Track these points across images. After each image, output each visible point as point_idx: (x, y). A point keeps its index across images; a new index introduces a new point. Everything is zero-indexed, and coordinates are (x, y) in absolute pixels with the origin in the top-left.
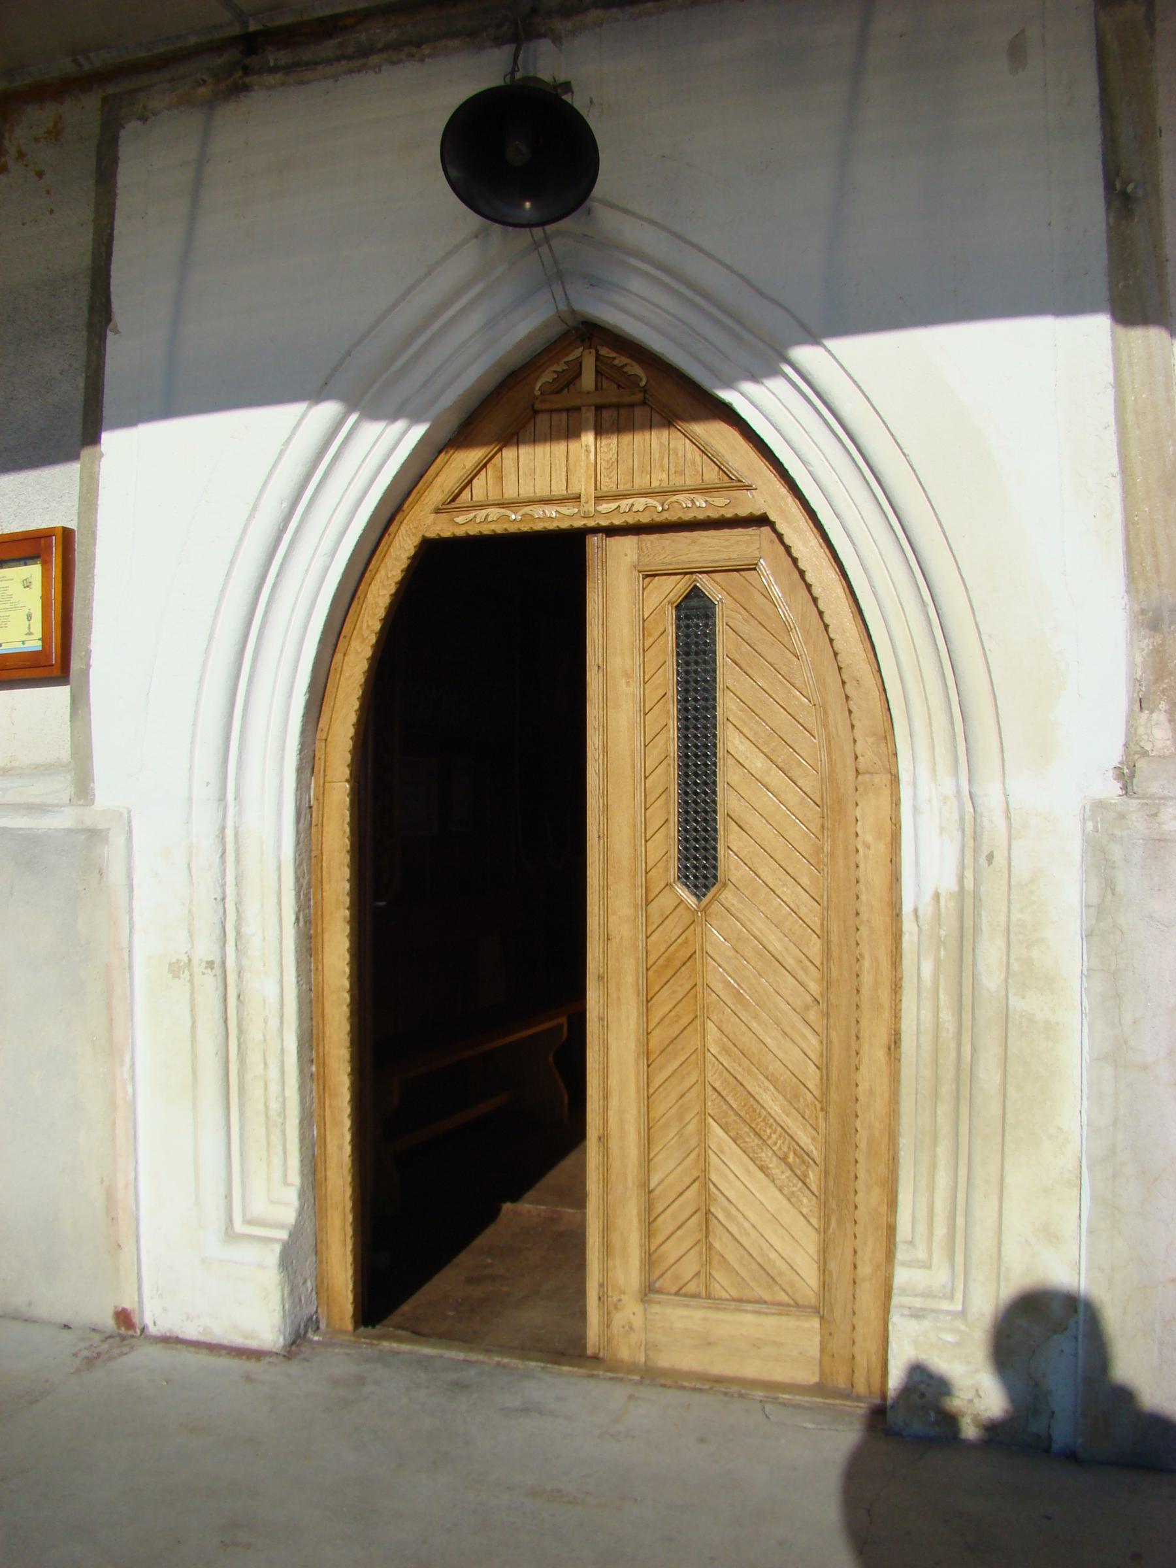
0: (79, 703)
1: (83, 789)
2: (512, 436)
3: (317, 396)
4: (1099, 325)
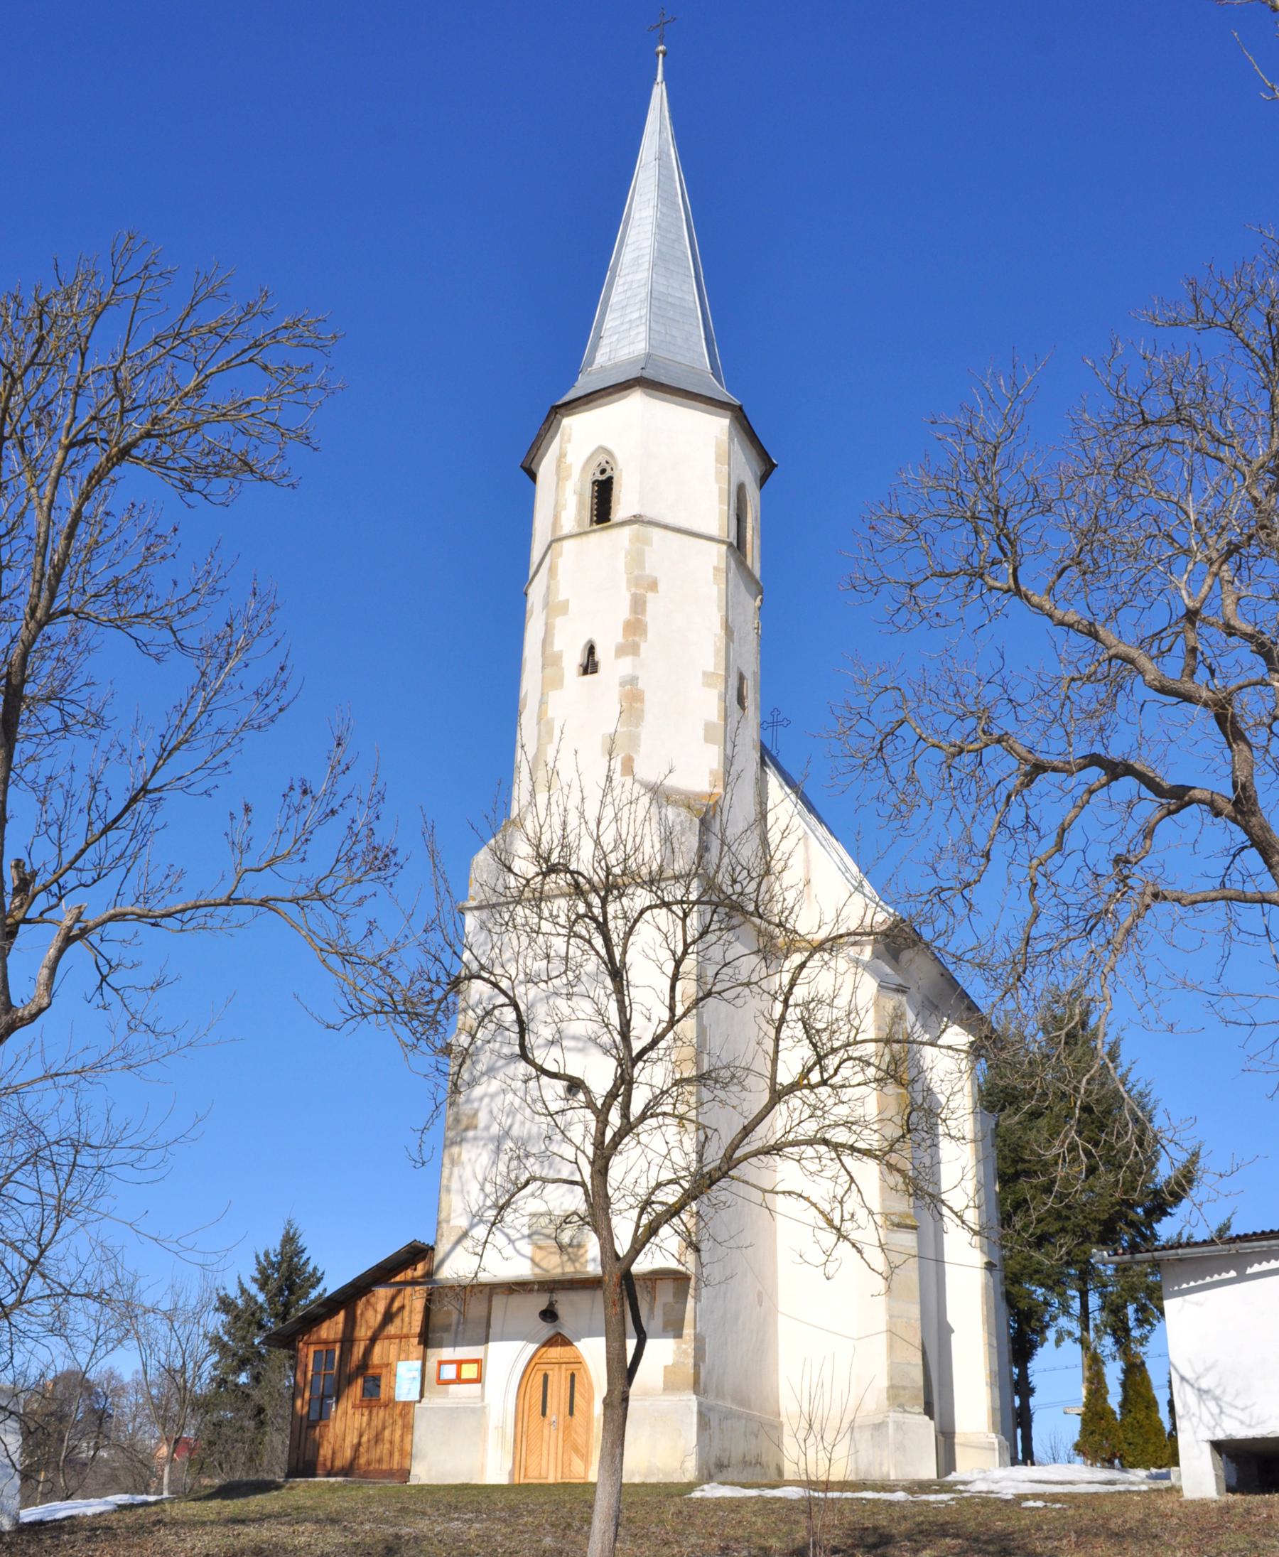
0: (483, 1387)
2: (551, 1346)
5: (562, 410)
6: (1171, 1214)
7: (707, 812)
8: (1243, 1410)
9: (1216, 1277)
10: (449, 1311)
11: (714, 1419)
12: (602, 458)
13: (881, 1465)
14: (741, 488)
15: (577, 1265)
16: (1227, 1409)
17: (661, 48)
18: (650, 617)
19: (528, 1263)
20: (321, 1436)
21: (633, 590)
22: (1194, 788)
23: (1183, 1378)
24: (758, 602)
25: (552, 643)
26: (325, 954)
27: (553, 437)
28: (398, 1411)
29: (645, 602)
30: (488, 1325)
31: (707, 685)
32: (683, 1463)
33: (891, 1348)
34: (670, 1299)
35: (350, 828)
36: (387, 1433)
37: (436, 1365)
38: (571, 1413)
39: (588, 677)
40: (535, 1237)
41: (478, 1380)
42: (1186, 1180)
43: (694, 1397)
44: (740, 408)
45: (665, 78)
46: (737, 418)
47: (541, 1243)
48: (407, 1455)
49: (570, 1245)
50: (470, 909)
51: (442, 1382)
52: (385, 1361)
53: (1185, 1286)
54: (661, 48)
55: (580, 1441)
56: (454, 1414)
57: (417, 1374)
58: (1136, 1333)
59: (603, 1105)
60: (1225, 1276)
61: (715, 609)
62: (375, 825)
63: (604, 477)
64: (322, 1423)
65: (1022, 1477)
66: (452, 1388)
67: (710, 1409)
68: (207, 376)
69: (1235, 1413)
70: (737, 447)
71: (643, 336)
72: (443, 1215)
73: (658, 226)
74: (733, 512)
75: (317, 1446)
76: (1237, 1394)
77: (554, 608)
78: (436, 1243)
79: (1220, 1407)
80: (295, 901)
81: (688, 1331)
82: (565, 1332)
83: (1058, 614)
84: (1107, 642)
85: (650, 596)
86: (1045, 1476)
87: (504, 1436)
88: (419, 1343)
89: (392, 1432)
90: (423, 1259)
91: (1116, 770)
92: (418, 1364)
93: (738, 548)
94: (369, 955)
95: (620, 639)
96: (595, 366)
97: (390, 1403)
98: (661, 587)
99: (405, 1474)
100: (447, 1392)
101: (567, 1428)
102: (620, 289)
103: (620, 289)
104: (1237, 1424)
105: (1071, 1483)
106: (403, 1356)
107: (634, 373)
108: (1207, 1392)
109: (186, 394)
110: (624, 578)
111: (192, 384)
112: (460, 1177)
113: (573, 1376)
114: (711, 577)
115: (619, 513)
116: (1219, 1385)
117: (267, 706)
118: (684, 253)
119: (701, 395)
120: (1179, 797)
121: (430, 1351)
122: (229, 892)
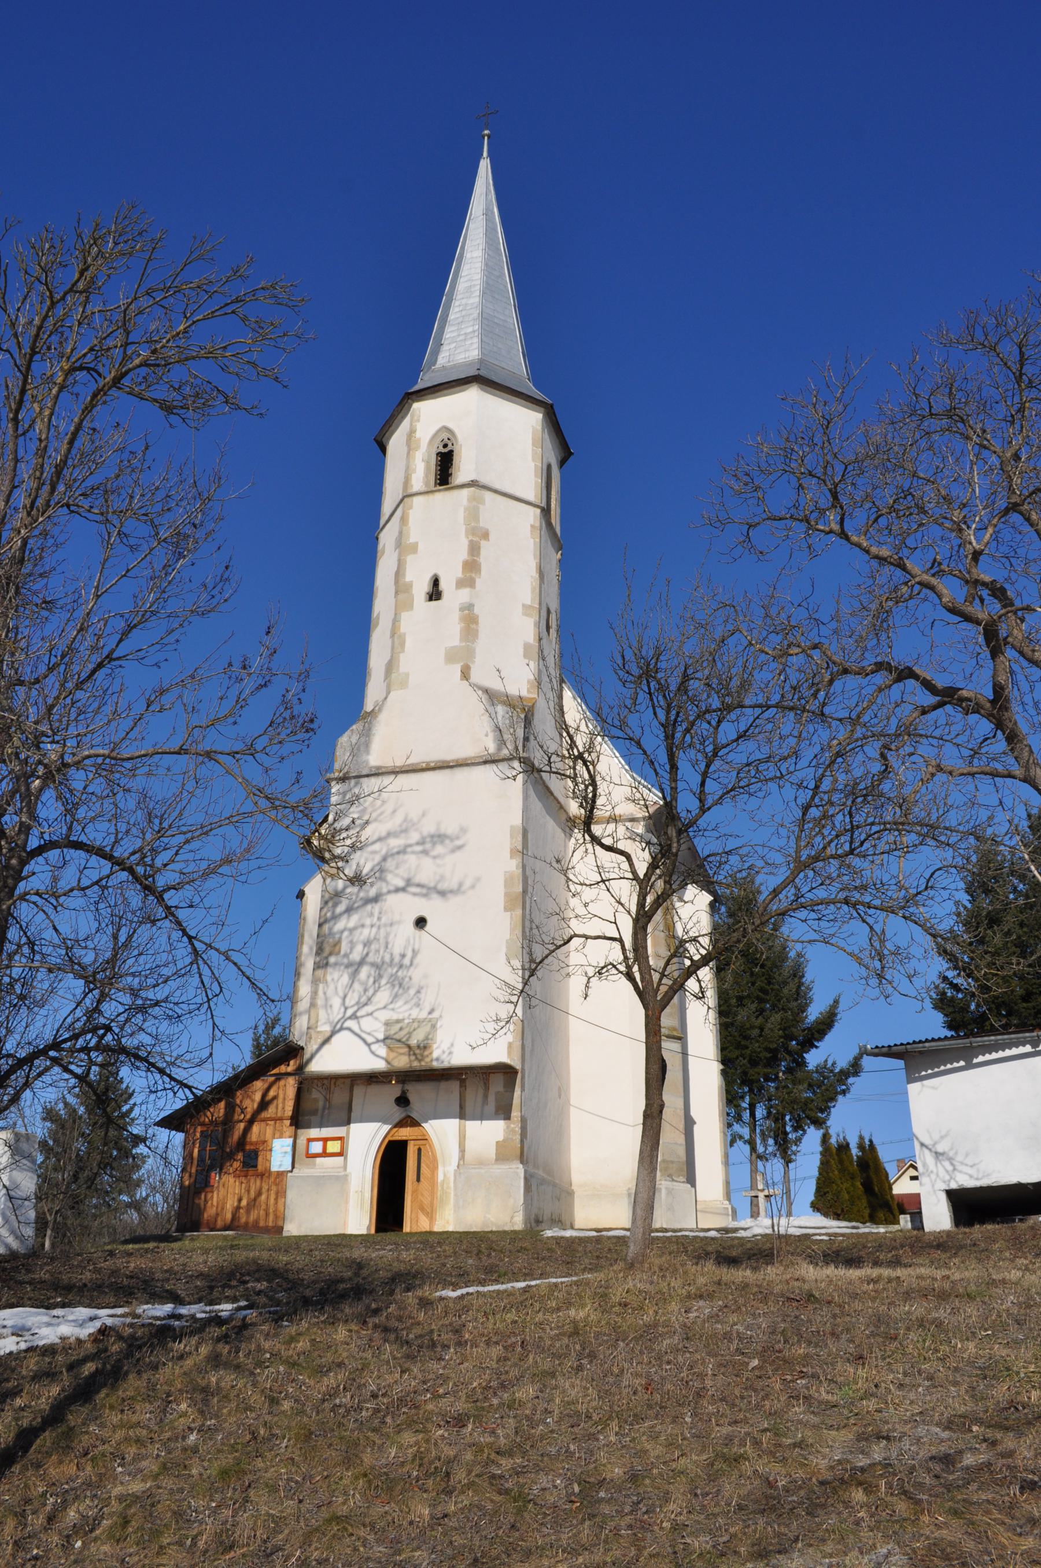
0: (346, 1159)
4: (457, 1120)
5: (414, 397)
6: (817, 1047)
9: (949, 1066)
11: (534, 1182)
12: (445, 435)
14: (549, 467)
16: (959, 1167)
17: (486, 132)
20: (206, 1201)
21: (471, 537)
23: (922, 1145)
24: (559, 556)
25: (404, 575)
26: (257, 798)
27: (403, 418)
28: (272, 1179)
29: (479, 548)
31: (525, 614)
32: (512, 1218)
34: (501, 1089)
35: (284, 696)
36: (263, 1197)
37: (305, 1142)
38: (418, 1180)
39: (433, 603)
40: (388, 1041)
42: (826, 1023)
43: (521, 1166)
44: (552, 406)
45: (489, 155)
48: (280, 1217)
49: (419, 1047)
52: (262, 1138)
53: (923, 1073)
55: (426, 1201)
56: (321, 1181)
57: (289, 1149)
58: (792, 1136)
59: (645, 875)
60: (956, 1065)
61: (532, 557)
62: (301, 696)
63: (446, 450)
66: (318, 1160)
67: (532, 1176)
68: (194, 322)
70: (546, 436)
71: (476, 345)
73: (486, 265)
74: (544, 485)
77: (404, 548)
80: (233, 754)
81: (515, 1114)
82: (414, 1115)
83: (874, 550)
84: (913, 572)
85: (483, 543)
86: (803, 1224)
87: (362, 1199)
88: (291, 1125)
90: (295, 1057)
91: (906, 674)
92: (290, 1141)
93: (546, 511)
94: (292, 800)
95: (460, 575)
96: (437, 366)
98: (492, 536)
100: (314, 1164)
102: (457, 310)
103: (457, 310)
104: (967, 1177)
107: (473, 372)
108: (942, 1154)
109: (178, 334)
110: (463, 528)
111: (182, 327)
112: (325, 993)
113: (419, 1150)
114: (529, 534)
116: (952, 1149)
117: (213, 597)
118: (506, 287)
119: (522, 394)
120: (948, 696)
121: (300, 1131)
122: (181, 743)
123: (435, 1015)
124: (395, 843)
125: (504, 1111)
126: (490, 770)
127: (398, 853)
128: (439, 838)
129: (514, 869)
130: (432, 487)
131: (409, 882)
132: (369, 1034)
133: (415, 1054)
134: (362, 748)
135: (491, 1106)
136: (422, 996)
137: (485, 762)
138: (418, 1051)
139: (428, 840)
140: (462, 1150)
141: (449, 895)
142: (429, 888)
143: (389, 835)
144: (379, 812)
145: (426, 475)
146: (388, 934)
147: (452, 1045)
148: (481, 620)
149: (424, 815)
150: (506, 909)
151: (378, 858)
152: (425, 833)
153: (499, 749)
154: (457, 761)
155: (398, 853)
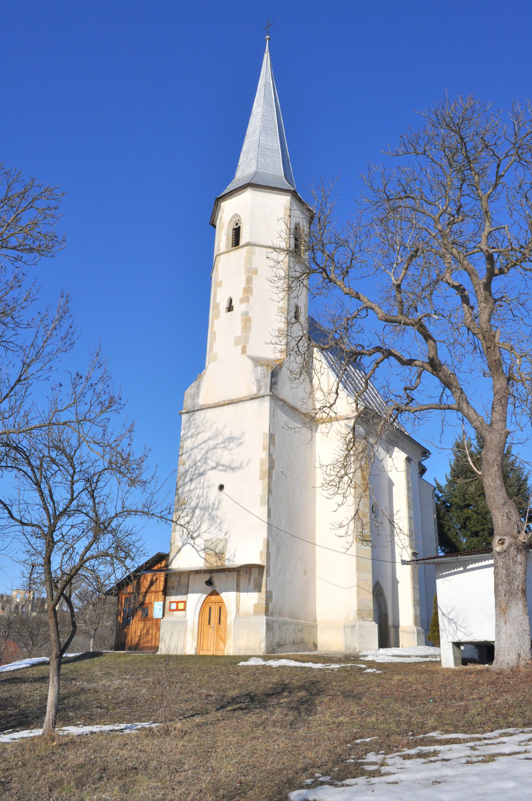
1: (186, 618)
2: (212, 595)
3: (201, 593)
4: (235, 593)
5: (220, 200)
7: (276, 367)
8: (465, 628)
10: (174, 582)
12: (236, 219)
13: (354, 643)
15: (222, 561)
16: (459, 628)
17: (267, 37)
18: (254, 286)
19: (203, 560)
21: (247, 274)
22: (416, 360)
23: (443, 614)
29: (252, 279)
30: (188, 587)
32: (260, 645)
33: (358, 593)
34: (257, 576)
37: (169, 603)
38: (219, 623)
40: (206, 550)
41: (184, 610)
43: (265, 617)
44: (294, 191)
46: (294, 196)
47: (209, 552)
48: (157, 640)
49: (220, 553)
50: (183, 413)
51: (171, 610)
53: (444, 573)
54: (267, 37)
55: (223, 635)
56: (175, 623)
57: (161, 607)
60: (459, 569)
63: (237, 227)
64: (128, 627)
65: (390, 653)
66: (175, 613)
69: (462, 630)
72: (172, 541)
75: (126, 636)
76: (463, 621)
78: (170, 553)
79: (456, 627)
81: (263, 589)
85: (254, 276)
87: (193, 634)
89: (153, 630)
90: (164, 560)
92: (162, 603)
96: (236, 179)
97: (152, 618)
99: (157, 648)
100: (173, 615)
101: (218, 629)
105: (409, 656)
106: (156, 600)
108: (452, 620)
113: (220, 608)
115: (242, 242)
116: (456, 617)
117: (66, 343)
119: (276, 188)
121: (167, 598)
123: (227, 536)
124: (212, 443)
125: (258, 588)
126: (256, 402)
127: (213, 448)
128: (231, 439)
129: (265, 456)
130: (231, 249)
131: (218, 464)
132: (198, 546)
133: (218, 556)
134: (196, 396)
135: (252, 586)
136: (222, 525)
137: (251, 399)
138: (219, 555)
139: (227, 440)
140: (238, 608)
141: (236, 470)
142: (227, 467)
143: (209, 439)
144: (204, 427)
145: (227, 243)
146: (207, 493)
147: (235, 551)
148: (253, 320)
149: (225, 427)
150: (261, 479)
151: (204, 452)
152: (225, 437)
153: (259, 390)
154: (238, 399)
155: (213, 448)
